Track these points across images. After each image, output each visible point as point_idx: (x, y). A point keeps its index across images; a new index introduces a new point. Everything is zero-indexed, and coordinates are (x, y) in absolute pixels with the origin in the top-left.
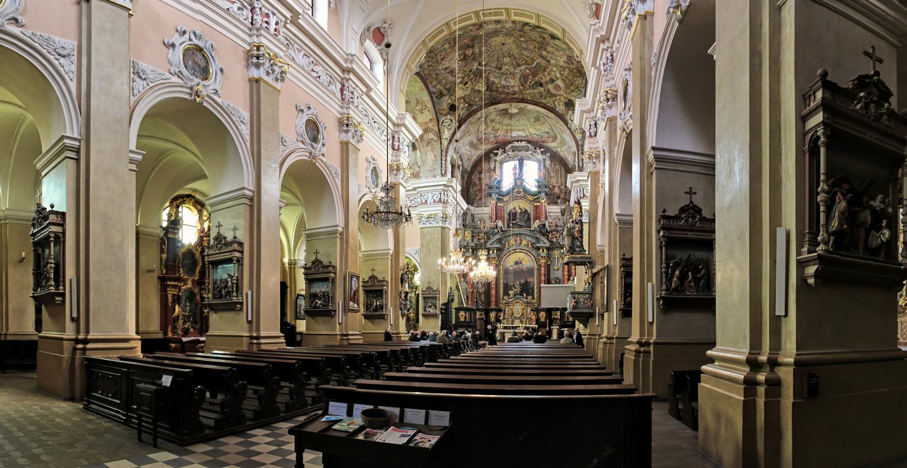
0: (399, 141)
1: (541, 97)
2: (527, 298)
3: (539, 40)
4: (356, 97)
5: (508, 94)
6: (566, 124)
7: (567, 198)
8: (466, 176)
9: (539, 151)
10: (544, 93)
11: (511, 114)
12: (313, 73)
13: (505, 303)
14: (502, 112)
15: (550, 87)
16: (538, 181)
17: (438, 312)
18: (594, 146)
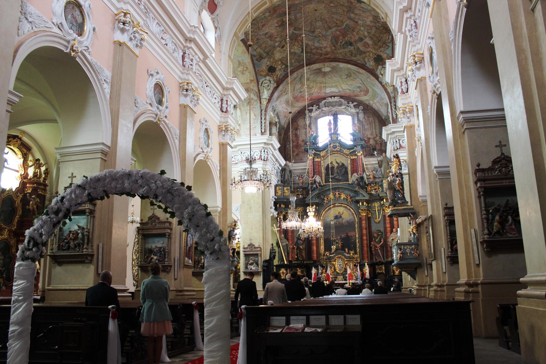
0: (227, 104)
1: (351, 55)
2: (349, 253)
3: (346, 4)
4: (195, 64)
5: (321, 55)
6: (377, 78)
7: (383, 148)
8: (283, 132)
9: (352, 105)
10: (354, 52)
11: (325, 72)
12: (162, 41)
13: (326, 259)
14: (317, 71)
15: (360, 45)
16: (353, 134)
17: (260, 269)
18: (407, 101)
